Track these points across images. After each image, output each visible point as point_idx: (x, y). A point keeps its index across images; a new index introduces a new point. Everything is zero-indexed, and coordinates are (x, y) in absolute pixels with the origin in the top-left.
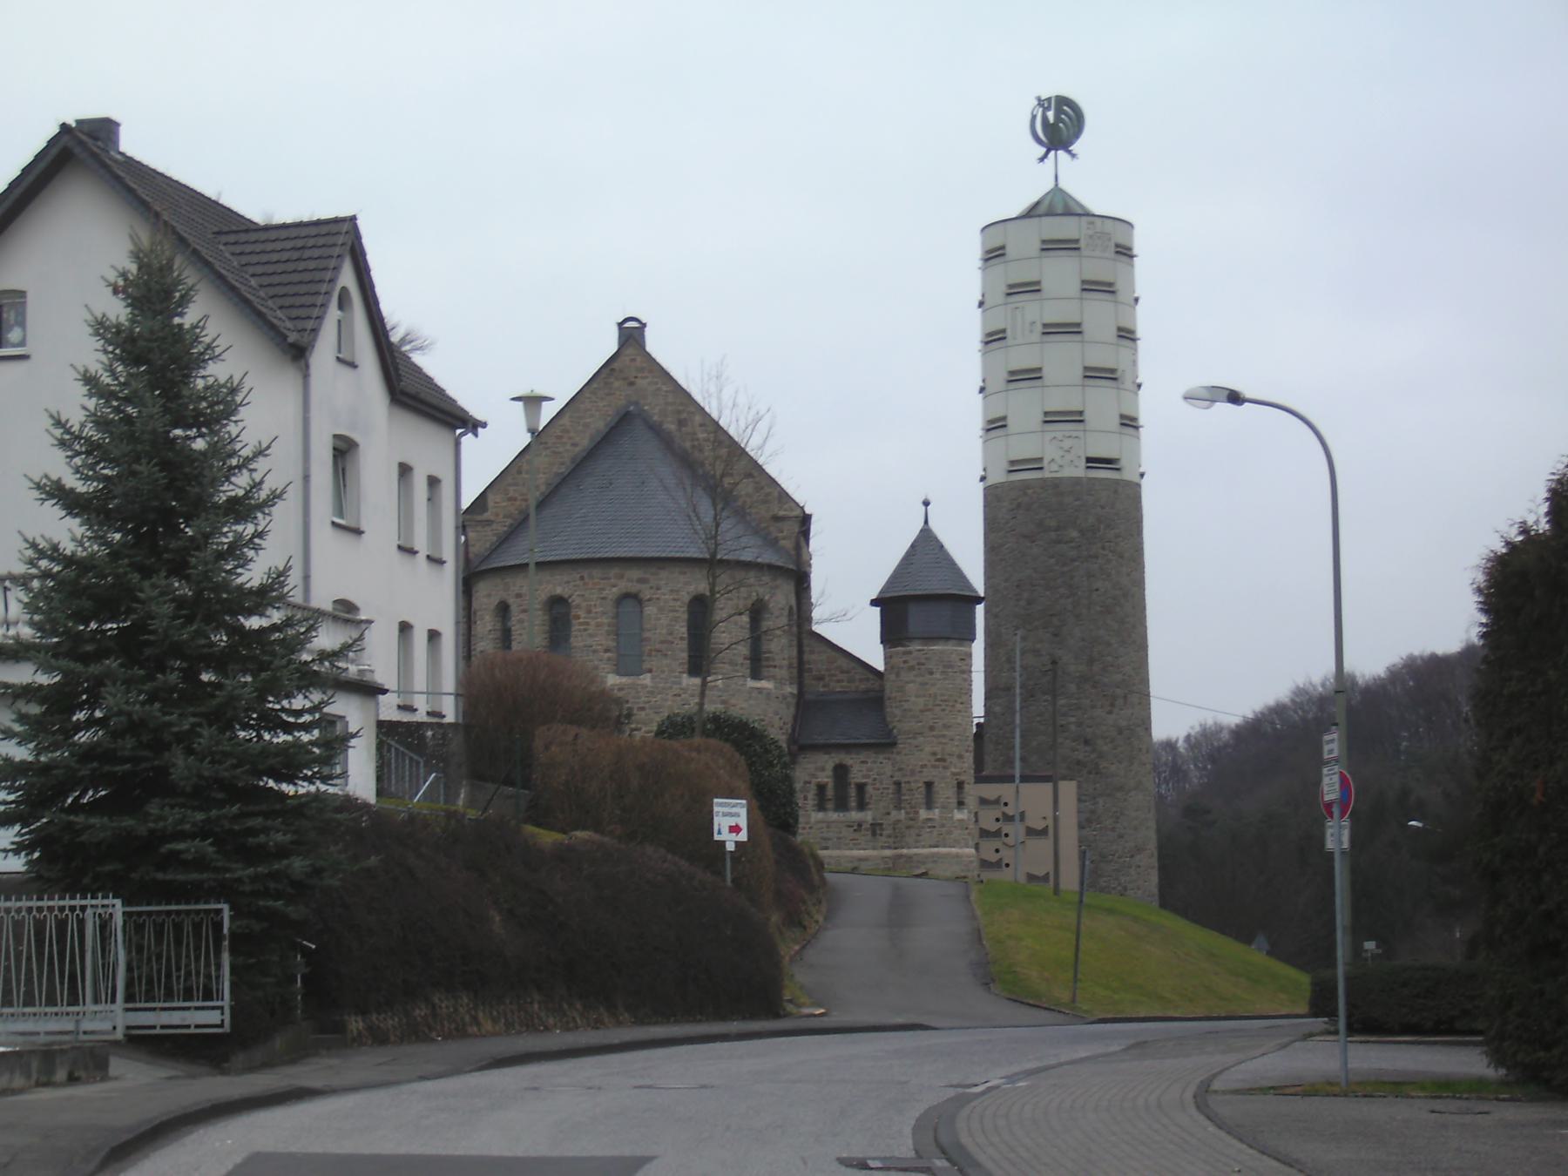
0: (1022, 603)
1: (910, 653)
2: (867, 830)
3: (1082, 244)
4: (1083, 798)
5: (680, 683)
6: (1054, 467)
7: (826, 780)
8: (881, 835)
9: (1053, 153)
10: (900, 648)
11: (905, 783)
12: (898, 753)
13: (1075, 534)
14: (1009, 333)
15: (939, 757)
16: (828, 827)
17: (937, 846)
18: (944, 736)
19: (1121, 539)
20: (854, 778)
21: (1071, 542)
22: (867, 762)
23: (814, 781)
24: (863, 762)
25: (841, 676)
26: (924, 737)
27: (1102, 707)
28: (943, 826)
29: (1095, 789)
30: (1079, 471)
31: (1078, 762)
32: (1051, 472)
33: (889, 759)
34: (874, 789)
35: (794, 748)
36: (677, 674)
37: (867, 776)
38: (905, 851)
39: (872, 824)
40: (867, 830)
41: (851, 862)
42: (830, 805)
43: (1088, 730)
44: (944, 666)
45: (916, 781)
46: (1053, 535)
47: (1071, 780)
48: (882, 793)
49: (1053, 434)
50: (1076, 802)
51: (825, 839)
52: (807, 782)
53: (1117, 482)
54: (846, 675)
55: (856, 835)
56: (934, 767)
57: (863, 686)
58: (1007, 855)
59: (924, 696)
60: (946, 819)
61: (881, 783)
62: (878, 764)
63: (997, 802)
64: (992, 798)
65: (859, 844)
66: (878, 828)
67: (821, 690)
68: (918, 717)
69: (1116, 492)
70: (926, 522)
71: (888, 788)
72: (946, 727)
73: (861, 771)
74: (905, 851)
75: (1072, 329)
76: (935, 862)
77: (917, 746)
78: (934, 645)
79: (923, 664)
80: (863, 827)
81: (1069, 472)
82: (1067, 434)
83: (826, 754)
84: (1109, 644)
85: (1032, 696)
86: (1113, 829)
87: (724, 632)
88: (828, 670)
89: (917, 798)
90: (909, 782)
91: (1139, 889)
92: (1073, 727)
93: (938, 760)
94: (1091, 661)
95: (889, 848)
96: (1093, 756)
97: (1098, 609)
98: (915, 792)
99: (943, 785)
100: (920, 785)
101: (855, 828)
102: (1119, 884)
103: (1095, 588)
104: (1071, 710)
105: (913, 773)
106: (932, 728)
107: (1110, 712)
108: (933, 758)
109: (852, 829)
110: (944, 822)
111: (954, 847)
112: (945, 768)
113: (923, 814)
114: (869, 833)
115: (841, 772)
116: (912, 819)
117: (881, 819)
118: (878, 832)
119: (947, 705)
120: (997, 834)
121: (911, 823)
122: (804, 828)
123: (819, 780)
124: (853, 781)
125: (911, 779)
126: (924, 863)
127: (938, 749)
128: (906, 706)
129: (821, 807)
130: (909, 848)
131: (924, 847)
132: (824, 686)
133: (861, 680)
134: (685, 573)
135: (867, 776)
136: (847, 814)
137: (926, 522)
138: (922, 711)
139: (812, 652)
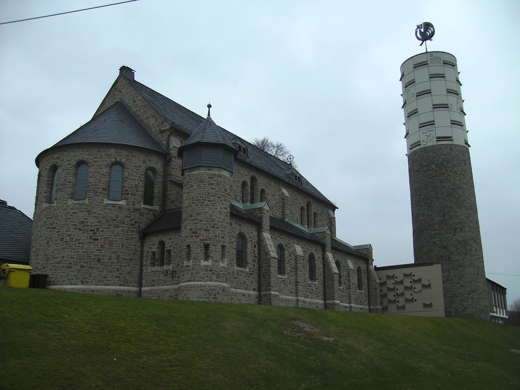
0: (417, 196)
2: (170, 274)
3: (429, 62)
4: (444, 271)
5: (67, 204)
6: (424, 143)
8: (175, 277)
9: (424, 42)
13: (434, 166)
16: (155, 274)
18: (197, 219)
19: (455, 167)
21: (433, 169)
27: (450, 233)
28: (194, 269)
29: (449, 267)
30: (435, 143)
31: (441, 256)
32: (424, 145)
36: (66, 199)
37: (171, 246)
39: (172, 272)
40: (170, 274)
43: (444, 243)
44: (198, 182)
46: (426, 168)
47: (439, 264)
49: (422, 131)
50: (441, 272)
51: (153, 281)
52: (148, 252)
53: (452, 145)
56: (191, 237)
58: (415, 296)
60: (196, 266)
63: (410, 275)
64: (408, 274)
69: (451, 149)
72: (198, 214)
76: (188, 290)
81: (430, 144)
84: (452, 208)
85: (422, 232)
86: (458, 283)
87: (91, 177)
88: (176, 198)
91: (473, 308)
92: (438, 242)
93: (193, 233)
94: (444, 215)
96: (447, 253)
97: (446, 194)
99: (195, 246)
102: (463, 306)
103: (444, 186)
104: (437, 235)
106: (191, 216)
107: (454, 235)
108: (190, 232)
109: (163, 275)
110: (195, 267)
111: (200, 281)
112: (196, 237)
113: (186, 263)
115: (162, 244)
117: (176, 269)
119: (199, 202)
120: (411, 288)
122: (146, 276)
127: (193, 227)
129: (153, 264)
132: (175, 206)
134: (74, 151)
138: (187, 207)
139: (171, 190)
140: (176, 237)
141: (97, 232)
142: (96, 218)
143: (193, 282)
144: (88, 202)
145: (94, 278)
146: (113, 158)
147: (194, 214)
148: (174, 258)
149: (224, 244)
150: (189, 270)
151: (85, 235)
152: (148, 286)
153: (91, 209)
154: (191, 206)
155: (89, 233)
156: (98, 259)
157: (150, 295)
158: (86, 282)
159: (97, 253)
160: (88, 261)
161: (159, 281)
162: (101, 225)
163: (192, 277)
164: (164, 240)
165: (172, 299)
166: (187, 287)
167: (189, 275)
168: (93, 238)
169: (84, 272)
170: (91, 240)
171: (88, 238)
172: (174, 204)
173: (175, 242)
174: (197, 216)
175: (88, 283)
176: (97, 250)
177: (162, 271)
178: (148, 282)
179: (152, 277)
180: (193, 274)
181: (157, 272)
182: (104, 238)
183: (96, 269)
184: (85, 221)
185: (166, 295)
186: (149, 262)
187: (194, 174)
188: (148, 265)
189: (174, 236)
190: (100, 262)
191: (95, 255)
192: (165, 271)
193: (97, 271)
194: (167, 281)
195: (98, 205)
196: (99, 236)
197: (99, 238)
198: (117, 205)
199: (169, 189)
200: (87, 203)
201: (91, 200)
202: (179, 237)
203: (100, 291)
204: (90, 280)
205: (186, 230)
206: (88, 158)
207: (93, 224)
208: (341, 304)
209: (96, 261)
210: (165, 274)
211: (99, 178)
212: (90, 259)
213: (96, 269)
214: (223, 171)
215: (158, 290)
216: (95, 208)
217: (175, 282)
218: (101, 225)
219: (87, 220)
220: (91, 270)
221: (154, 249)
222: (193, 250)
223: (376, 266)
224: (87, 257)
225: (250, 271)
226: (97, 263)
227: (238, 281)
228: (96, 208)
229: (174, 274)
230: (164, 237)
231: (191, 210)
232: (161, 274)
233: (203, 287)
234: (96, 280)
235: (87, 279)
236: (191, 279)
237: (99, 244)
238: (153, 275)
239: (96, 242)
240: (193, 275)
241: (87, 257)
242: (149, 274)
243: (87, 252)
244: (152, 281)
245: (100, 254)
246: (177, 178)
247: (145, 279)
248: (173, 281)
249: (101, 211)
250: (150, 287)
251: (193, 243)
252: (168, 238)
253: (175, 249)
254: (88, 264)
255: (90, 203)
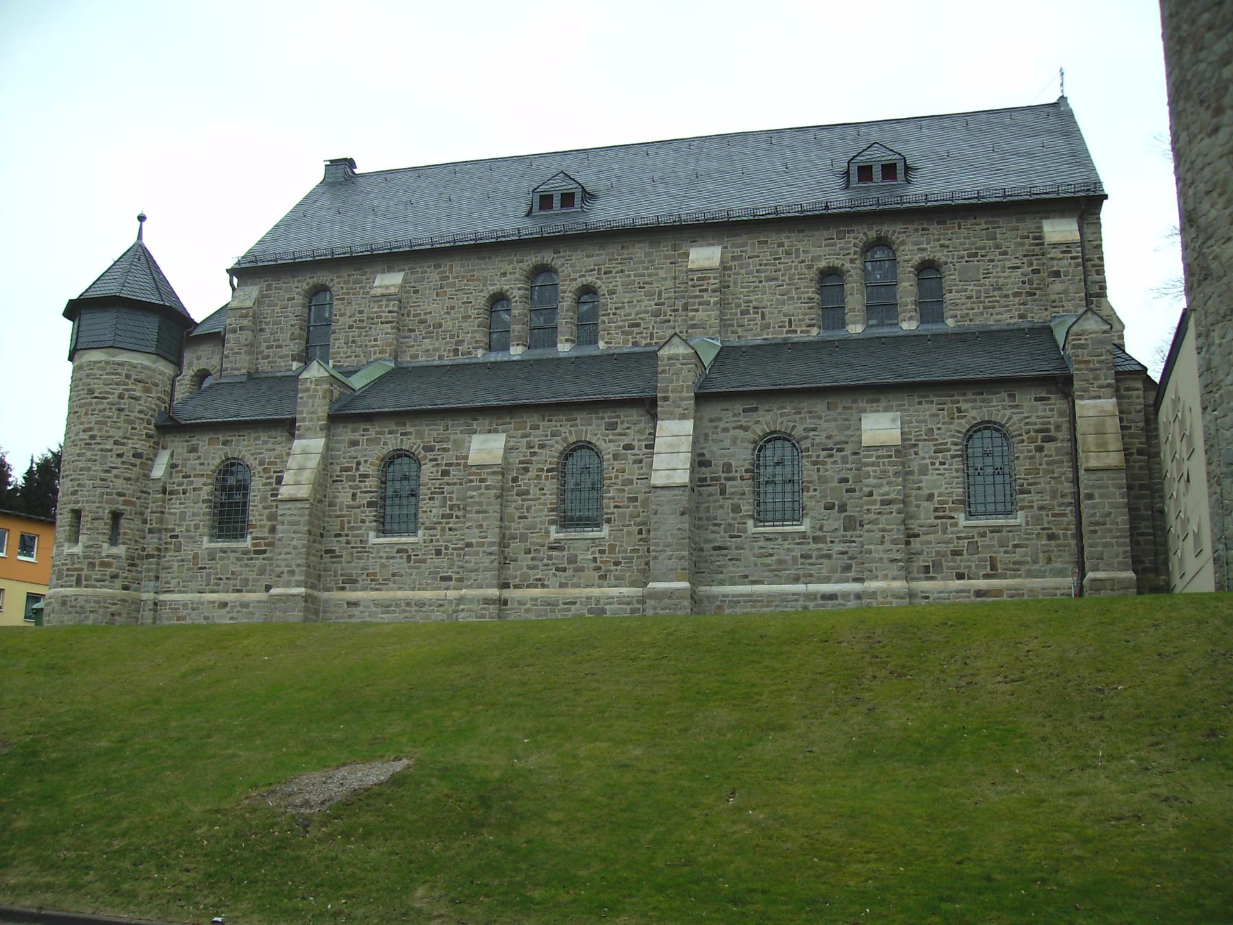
149: (77, 507)
208: (44, 853)
214: (84, 354)
223: (350, 163)
225: (254, 545)
227: (209, 575)
233: (414, 563)
246: (236, 373)
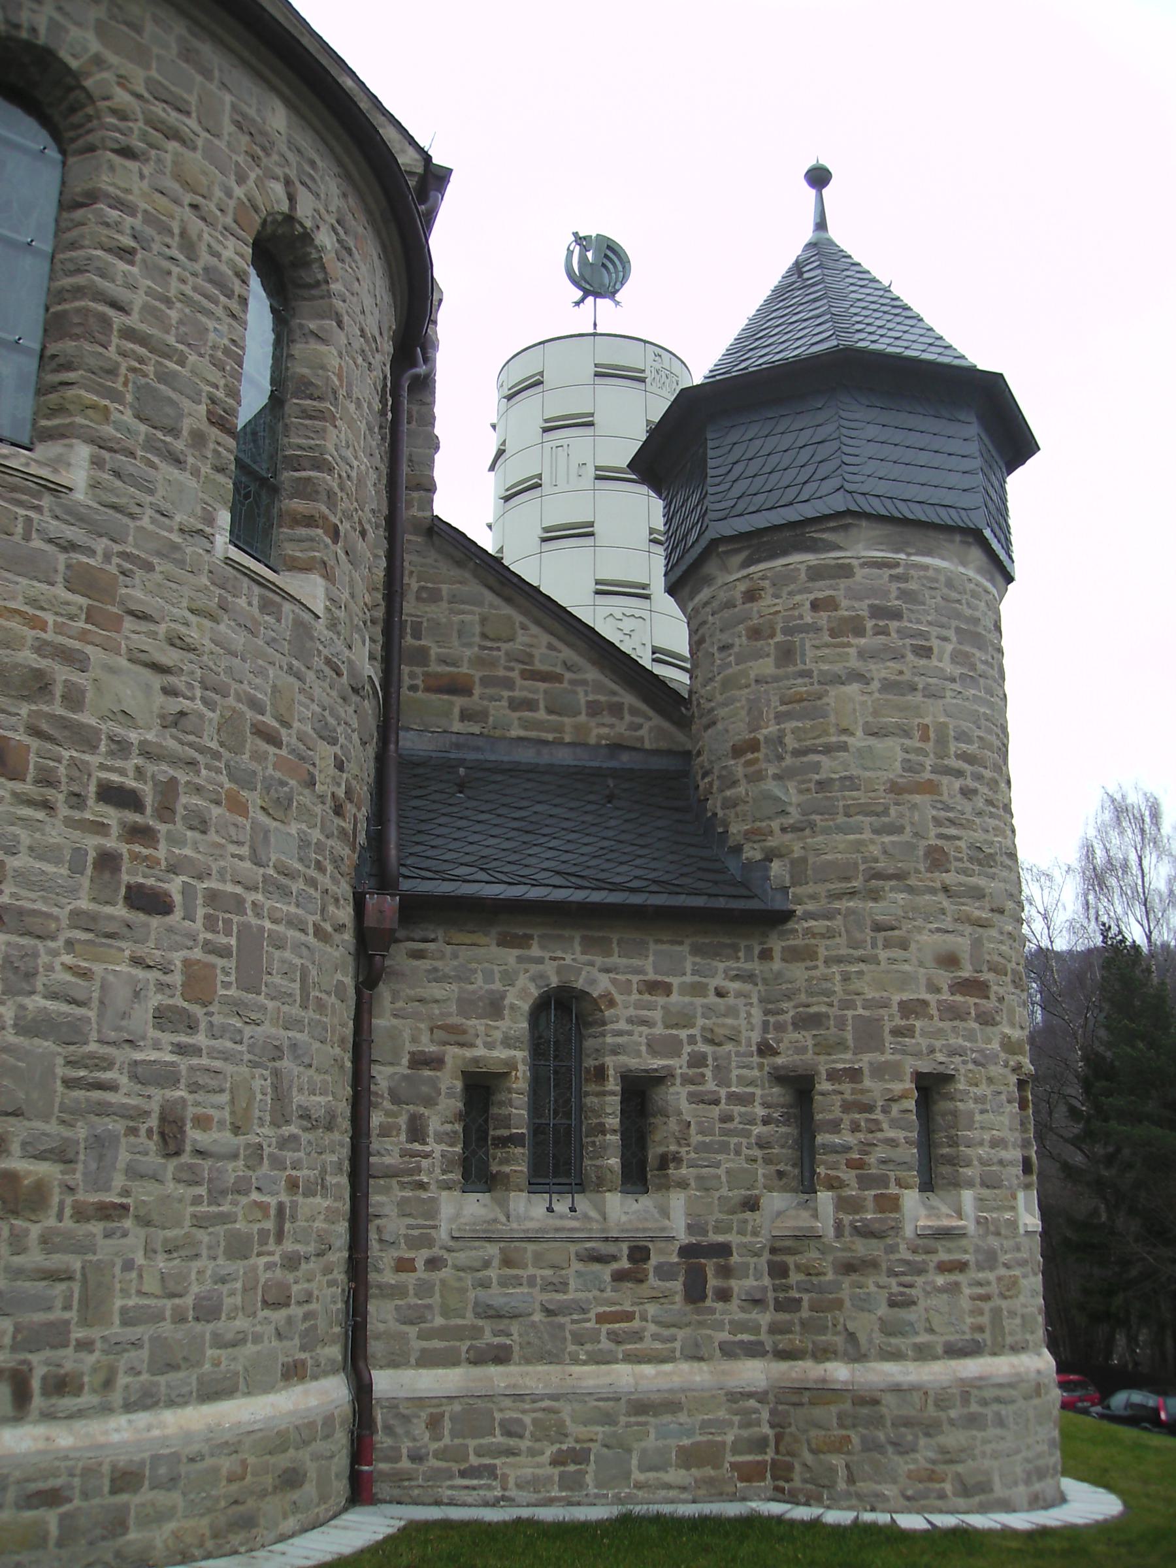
1: (845, 571)
2: (665, 1272)
7: (502, 1053)
8: (724, 1295)
10: (795, 558)
11: (833, 1076)
12: (793, 955)
14: (545, 480)
15: (966, 973)
16: (507, 1262)
17: (971, 1350)
20: (615, 1051)
22: (667, 989)
23: (453, 1055)
24: (653, 987)
25: (524, 689)
26: (911, 890)
28: (990, 1260)
33: (749, 978)
34: (697, 1099)
35: (383, 906)
38: (840, 1372)
39: (686, 1251)
40: (665, 1272)
41: (608, 1419)
42: (517, 1163)
45: (879, 1071)
48: (726, 1118)
51: (493, 1314)
52: (420, 1061)
54: (542, 686)
55: (625, 1298)
56: (954, 1013)
57: (600, 731)
59: (907, 734)
61: (723, 1082)
62: (712, 999)
65: (637, 1336)
66: (710, 1266)
67: (457, 726)
68: (886, 812)
70: (821, 225)
71: (745, 1100)
73: (644, 1022)
74: (840, 1372)
75: (583, 531)
76: (973, 1421)
77: (878, 928)
78: (929, 553)
79: (897, 615)
80: (654, 1261)
82: (628, 612)
83: (505, 942)
88: (479, 662)
89: (892, 1143)
90: (854, 1075)
95: (754, 1351)
98: (878, 1115)
99: (983, 1089)
100: (897, 1087)
101: (625, 1264)
105: (869, 1035)
106: (937, 859)
108: (944, 978)
114: (678, 1285)
116: (866, 1232)
118: (712, 1282)
121: (862, 1248)
122: (404, 1266)
123: (480, 1052)
124: (610, 1061)
125: (865, 1061)
126: (931, 1428)
127: (961, 943)
128: (829, 766)
130: (857, 1356)
131: (923, 1354)
132: (465, 716)
133: (594, 709)
135: (672, 1047)
136: (583, 1203)
137: (821, 225)
138: (895, 788)
139: (434, 597)
140: (713, 983)
141: (162, 828)
142: (157, 681)
143: (994, 1354)
144: (95, 485)
145: (125, 1323)
146: (276, 178)
147: (958, 849)
148: (702, 1148)
150: (962, 1267)
151: (56, 833)
152: (428, 1360)
153: (113, 569)
154: (931, 788)
155: (88, 816)
156: (163, 1119)
157: (472, 1443)
158: (61, 1385)
159: (157, 1046)
160: (81, 1132)
161: (562, 1319)
162: (192, 763)
163: (985, 1320)
164: (593, 982)
165: (709, 1472)
166: (965, 1397)
167: (965, 1304)
168: (129, 887)
169: (35, 1258)
170: (113, 904)
171: (76, 868)
172: (459, 702)
173: (700, 1022)
174: (976, 868)
175: (78, 1391)
176: (163, 1018)
177: (589, 1239)
178: (439, 1321)
179: (485, 1284)
180: (987, 1298)
181: (531, 1247)
182: (213, 897)
183: (145, 1222)
184: (62, 674)
185: (651, 1442)
186: (435, 1148)
187: (930, 573)
188: (432, 1171)
189: (689, 967)
190: (177, 1154)
191: (142, 1075)
192: (617, 1239)
193: (149, 1251)
194: (636, 1324)
195: (175, 547)
196: (173, 869)
197: (174, 887)
198: (287, 607)
199: (415, 586)
200: (80, 496)
201: (117, 474)
202: (736, 986)
203: (183, 1469)
204: (91, 1359)
205: (897, 953)
206: (98, 62)
207: (133, 736)
209: (150, 1132)
210: (615, 1266)
211: (188, 290)
212: (103, 1110)
213: (148, 1223)
215: (554, 1397)
216: (149, 567)
217: (724, 1336)
218: (192, 763)
219: (77, 678)
220: (100, 1241)
221: (490, 1046)
222: (978, 1117)
224: (69, 1083)
226: (153, 1160)
228: (157, 577)
229: (710, 1272)
230: (599, 960)
231: (937, 822)
232: (577, 1266)
234: (145, 1353)
235: (65, 1345)
236: (978, 1337)
237: (177, 957)
238: (487, 1264)
239: (146, 925)
240: (986, 1306)
241: (69, 1083)
242: (436, 1251)
243: (70, 1033)
244: (478, 1315)
245: (184, 1064)
247: (399, 1291)
248: (701, 1324)
249: (193, 619)
250: (455, 1363)
251: (971, 1066)
252: (635, 979)
253: (708, 1073)
254: (80, 1167)
255: (114, 507)
